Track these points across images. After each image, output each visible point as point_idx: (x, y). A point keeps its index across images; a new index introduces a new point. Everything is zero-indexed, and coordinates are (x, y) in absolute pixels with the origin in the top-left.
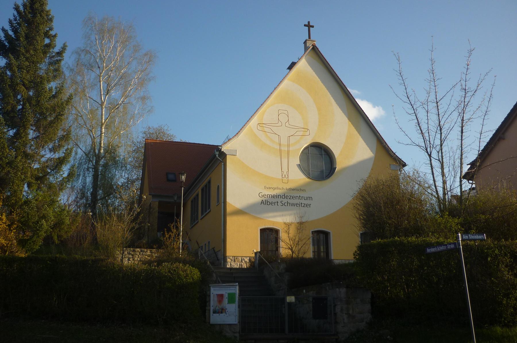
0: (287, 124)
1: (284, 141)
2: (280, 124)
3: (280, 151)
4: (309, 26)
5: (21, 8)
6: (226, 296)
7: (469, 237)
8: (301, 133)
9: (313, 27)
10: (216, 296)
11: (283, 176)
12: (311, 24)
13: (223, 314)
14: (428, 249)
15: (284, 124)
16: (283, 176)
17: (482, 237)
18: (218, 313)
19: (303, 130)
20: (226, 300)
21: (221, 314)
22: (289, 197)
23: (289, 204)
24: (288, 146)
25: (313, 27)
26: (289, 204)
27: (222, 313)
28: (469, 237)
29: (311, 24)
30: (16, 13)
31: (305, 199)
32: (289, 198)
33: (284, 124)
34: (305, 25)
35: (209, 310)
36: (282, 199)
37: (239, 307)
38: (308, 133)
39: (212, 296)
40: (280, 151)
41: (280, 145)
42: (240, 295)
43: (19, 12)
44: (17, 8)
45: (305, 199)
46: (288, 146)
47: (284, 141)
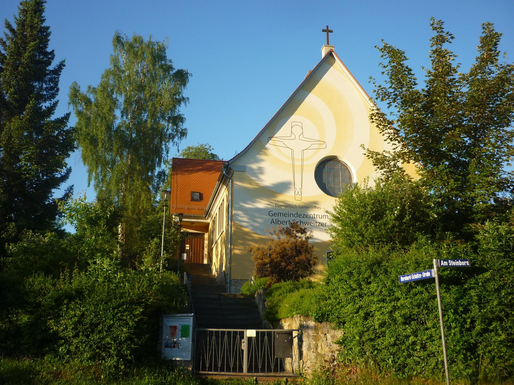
0: (301, 137)
1: (298, 156)
2: (293, 137)
3: (293, 166)
4: (328, 31)
5: (15, 27)
6: (180, 328)
7: (448, 263)
8: (317, 146)
9: (331, 32)
10: (169, 328)
11: (296, 193)
12: (329, 29)
13: (176, 349)
14: (401, 277)
15: (297, 138)
16: (296, 193)
17: (466, 263)
18: (171, 347)
19: (318, 142)
20: (179, 332)
21: (173, 349)
22: (303, 215)
23: (302, 223)
24: (302, 160)
25: (331, 32)
26: (302, 223)
27: (174, 347)
28: (448, 263)
29: (329, 29)
30: (8, 32)
31: (320, 217)
32: (302, 216)
33: (297, 138)
34: (323, 31)
35: (161, 344)
36: (294, 218)
37: (193, 341)
38: (324, 146)
39: (164, 328)
40: (293, 166)
41: (293, 159)
42: (194, 328)
43: (12, 30)
44: (9, 26)
45: (320, 217)
46: (302, 160)
47: (298, 156)
